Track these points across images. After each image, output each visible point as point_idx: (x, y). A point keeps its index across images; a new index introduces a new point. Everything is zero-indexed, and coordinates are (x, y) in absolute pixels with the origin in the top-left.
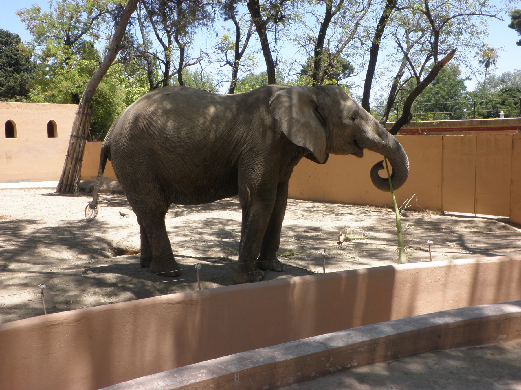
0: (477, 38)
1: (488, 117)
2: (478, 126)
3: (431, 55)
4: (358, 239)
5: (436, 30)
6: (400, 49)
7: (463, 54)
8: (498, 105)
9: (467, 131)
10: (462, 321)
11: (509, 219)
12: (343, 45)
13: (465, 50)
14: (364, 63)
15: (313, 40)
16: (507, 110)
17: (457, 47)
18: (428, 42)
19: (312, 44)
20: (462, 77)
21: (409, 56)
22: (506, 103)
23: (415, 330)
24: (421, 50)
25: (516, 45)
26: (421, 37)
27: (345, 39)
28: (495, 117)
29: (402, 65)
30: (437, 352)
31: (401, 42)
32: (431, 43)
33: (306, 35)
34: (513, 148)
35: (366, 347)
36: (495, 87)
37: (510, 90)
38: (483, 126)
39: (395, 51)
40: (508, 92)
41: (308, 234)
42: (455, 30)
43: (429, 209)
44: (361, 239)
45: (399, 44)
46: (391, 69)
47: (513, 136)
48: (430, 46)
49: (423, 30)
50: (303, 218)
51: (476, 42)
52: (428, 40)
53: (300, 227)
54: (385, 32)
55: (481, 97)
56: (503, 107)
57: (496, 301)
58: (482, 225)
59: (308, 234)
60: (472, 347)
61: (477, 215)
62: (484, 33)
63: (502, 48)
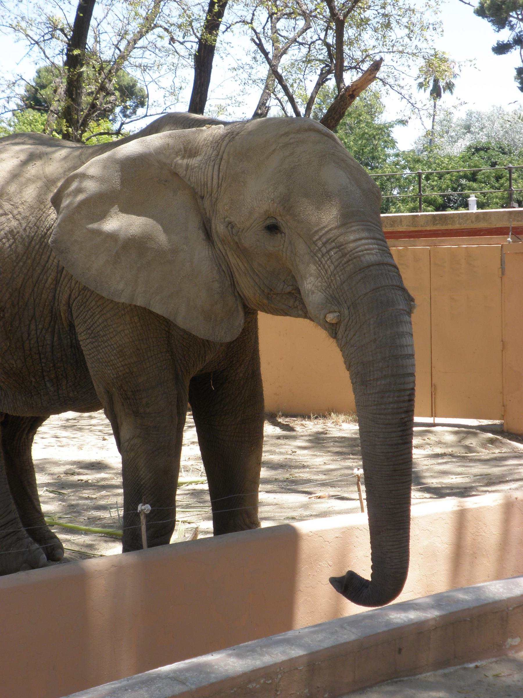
0: (422, 39)
1: (444, 207)
2: (428, 228)
3: (329, 72)
4: (191, 483)
5: (338, 18)
6: (260, 56)
7: (393, 71)
8: (463, 182)
9: (409, 237)
10: (440, 616)
11: (502, 425)
12: (129, 42)
13: (399, 63)
14: (178, 85)
15: (62, 30)
16: (481, 193)
17: (382, 55)
18: (320, 42)
19: (58, 39)
20: (382, 119)
21: (280, 70)
22: (479, 177)
23: (354, 641)
24: (308, 60)
25: (492, 53)
26: (304, 30)
27: (134, 27)
28: (456, 209)
29: (264, 91)
30: (396, 682)
31: (263, 41)
32: (328, 45)
33: (44, 18)
34: (503, 273)
35: (262, 681)
36: (454, 141)
37: (486, 149)
38: (438, 227)
39: (248, 60)
40: (482, 153)
41: (76, 478)
42: (376, 20)
43: (338, 412)
44: (197, 483)
45: (260, 46)
46: (240, 99)
47: (502, 247)
48: (325, 50)
49: (307, 16)
50: (59, 444)
51: (419, 46)
52: (320, 39)
53: (56, 464)
54: (228, 17)
55: (429, 164)
56: (475, 185)
57: (499, 576)
58: (450, 438)
59: (76, 478)
60: (459, 667)
61: (438, 420)
62: (435, 29)
63: (471, 61)
